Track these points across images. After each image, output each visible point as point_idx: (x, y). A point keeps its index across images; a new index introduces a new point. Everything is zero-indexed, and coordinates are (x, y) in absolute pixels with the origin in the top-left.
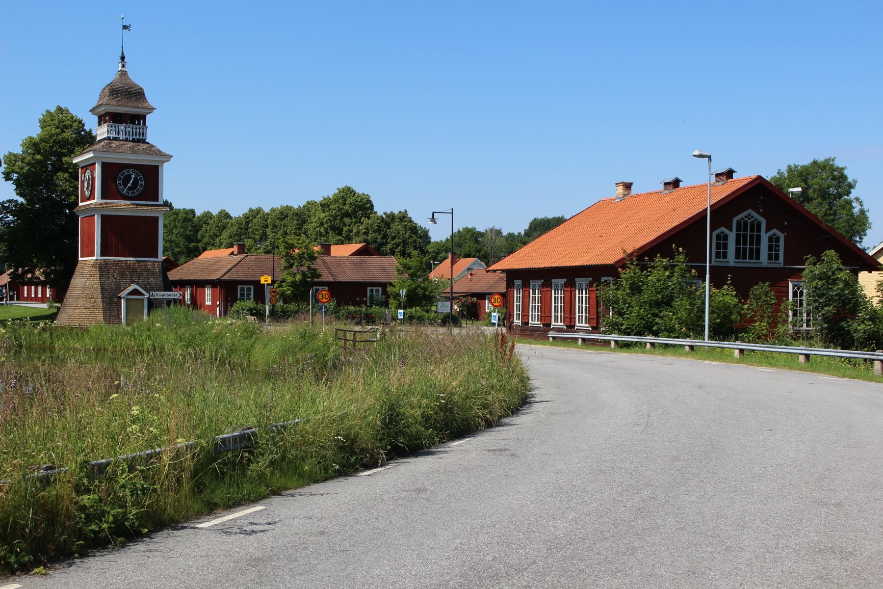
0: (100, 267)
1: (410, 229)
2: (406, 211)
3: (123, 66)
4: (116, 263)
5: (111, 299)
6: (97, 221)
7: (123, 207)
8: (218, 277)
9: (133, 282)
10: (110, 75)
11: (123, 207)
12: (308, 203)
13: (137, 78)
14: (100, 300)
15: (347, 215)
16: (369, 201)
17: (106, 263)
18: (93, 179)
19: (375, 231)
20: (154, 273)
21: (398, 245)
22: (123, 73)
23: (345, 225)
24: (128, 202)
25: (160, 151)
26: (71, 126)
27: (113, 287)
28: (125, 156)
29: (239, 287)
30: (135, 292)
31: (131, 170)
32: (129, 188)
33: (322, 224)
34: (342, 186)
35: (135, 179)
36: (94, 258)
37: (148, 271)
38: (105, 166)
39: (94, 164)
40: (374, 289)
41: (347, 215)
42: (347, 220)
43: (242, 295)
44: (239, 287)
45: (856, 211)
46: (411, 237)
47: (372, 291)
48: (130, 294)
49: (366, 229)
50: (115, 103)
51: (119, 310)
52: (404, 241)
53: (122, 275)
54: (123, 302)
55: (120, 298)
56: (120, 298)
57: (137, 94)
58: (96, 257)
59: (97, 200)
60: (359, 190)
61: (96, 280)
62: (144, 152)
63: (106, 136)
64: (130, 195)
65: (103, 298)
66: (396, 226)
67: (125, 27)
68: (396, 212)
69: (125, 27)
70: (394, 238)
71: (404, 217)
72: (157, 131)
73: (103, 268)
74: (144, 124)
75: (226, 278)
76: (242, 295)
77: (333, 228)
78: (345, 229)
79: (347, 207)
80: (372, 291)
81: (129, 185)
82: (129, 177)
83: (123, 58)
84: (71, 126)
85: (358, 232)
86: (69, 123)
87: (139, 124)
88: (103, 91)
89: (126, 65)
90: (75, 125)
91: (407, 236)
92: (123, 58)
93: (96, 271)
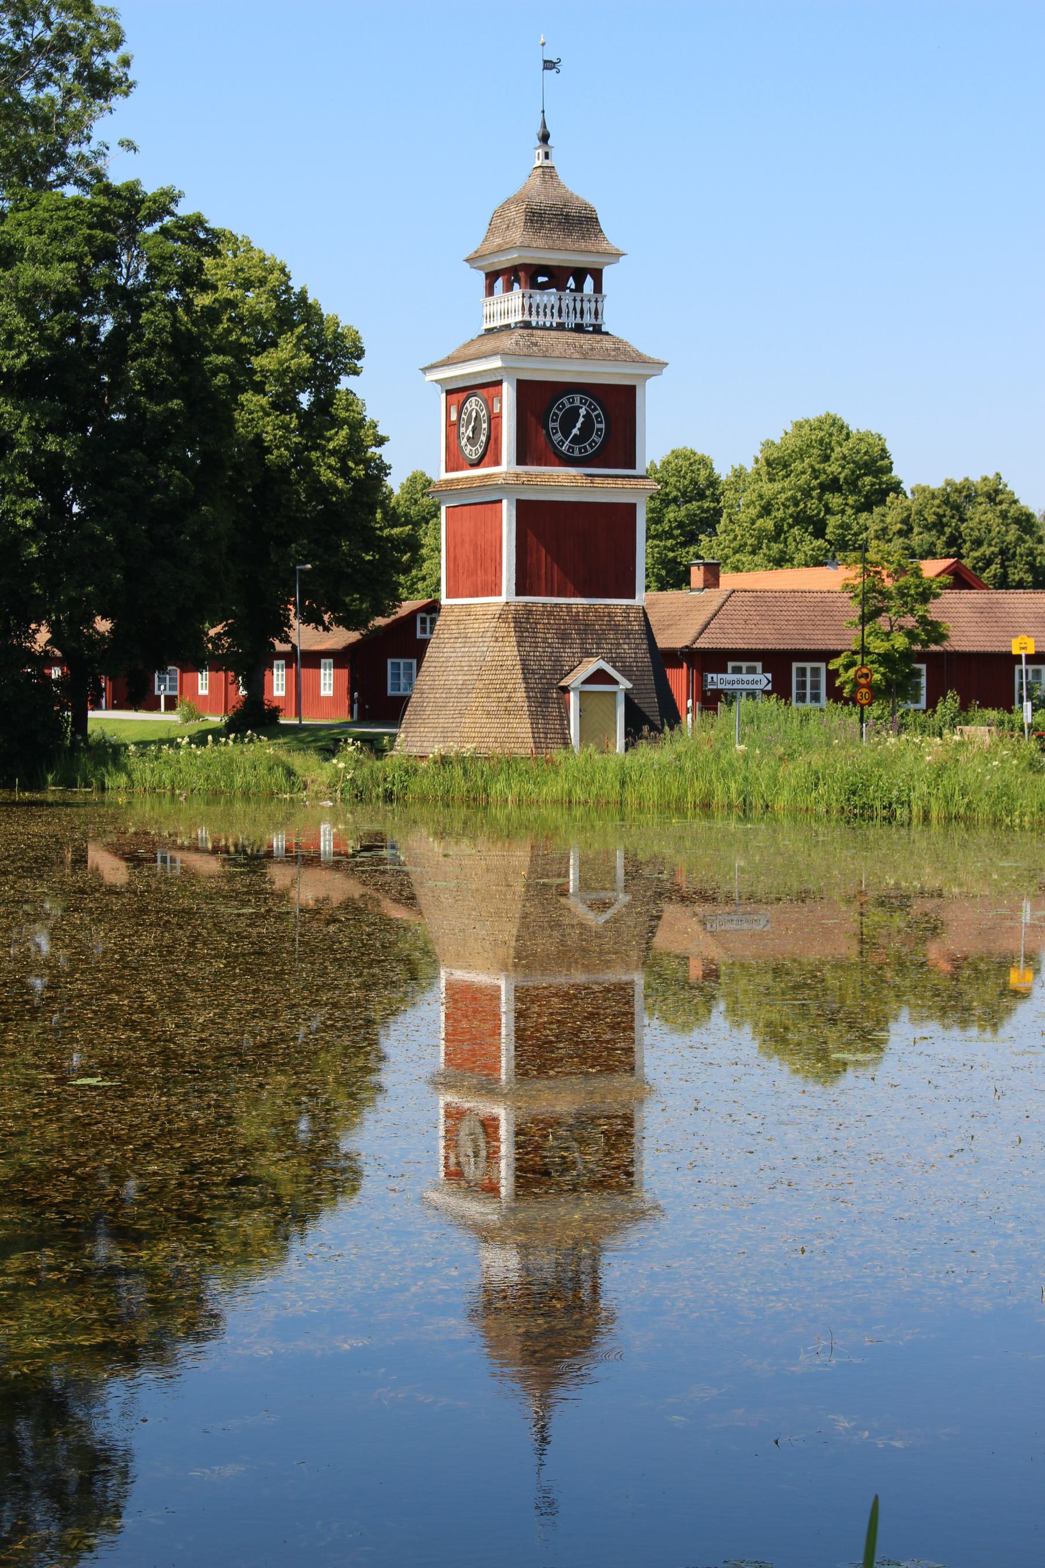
0: (516, 620)
1: (1017, 521)
2: (998, 477)
3: (547, 156)
4: (551, 612)
5: (545, 691)
6: (507, 513)
7: (564, 482)
8: (686, 642)
9: (589, 654)
10: (514, 175)
11: (564, 482)
12: (676, 455)
13: (580, 184)
14: (520, 695)
15: (833, 485)
16: (884, 454)
17: (529, 610)
18: (494, 419)
19: (928, 528)
20: (628, 634)
21: (989, 562)
22: (548, 172)
23: (828, 510)
24: (572, 471)
25: (640, 355)
26: (262, 282)
27: (548, 665)
28: (566, 364)
29: (795, 665)
30: (600, 677)
31: (577, 398)
32: (576, 440)
33: (766, 510)
34: (814, 413)
35: (587, 416)
36: (502, 599)
37: (616, 628)
38: (524, 388)
39: (499, 383)
40: (808, 666)
41: (833, 485)
42: (835, 500)
43: (802, 685)
44: (795, 665)
45: (329, 336)
46: (1021, 540)
47: (802, 672)
48: (588, 681)
49: (906, 521)
50: (540, 243)
51: (564, 717)
52: (1003, 552)
53: (564, 636)
54: (573, 698)
55: (565, 690)
56: (565, 690)
57: (580, 222)
58: (507, 593)
59: (507, 464)
60: (857, 423)
61: (510, 651)
62: (607, 356)
63: (519, 318)
64: (576, 454)
65: (528, 690)
66: (979, 515)
67: (549, 65)
68: (976, 478)
69: (549, 65)
70: (978, 543)
71: (997, 492)
72: (626, 307)
73: (523, 623)
74: (598, 288)
75: (702, 644)
76: (802, 685)
77: (801, 519)
78: (832, 521)
79: (833, 468)
80: (802, 672)
81: (575, 431)
82: (574, 413)
83: (545, 138)
84: (262, 282)
85: (884, 530)
86: (260, 273)
87: (579, 288)
88: (500, 213)
89: (553, 154)
90: (274, 278)
91: (1011, 537)
92: (545, 138)
93: (508, 631)
